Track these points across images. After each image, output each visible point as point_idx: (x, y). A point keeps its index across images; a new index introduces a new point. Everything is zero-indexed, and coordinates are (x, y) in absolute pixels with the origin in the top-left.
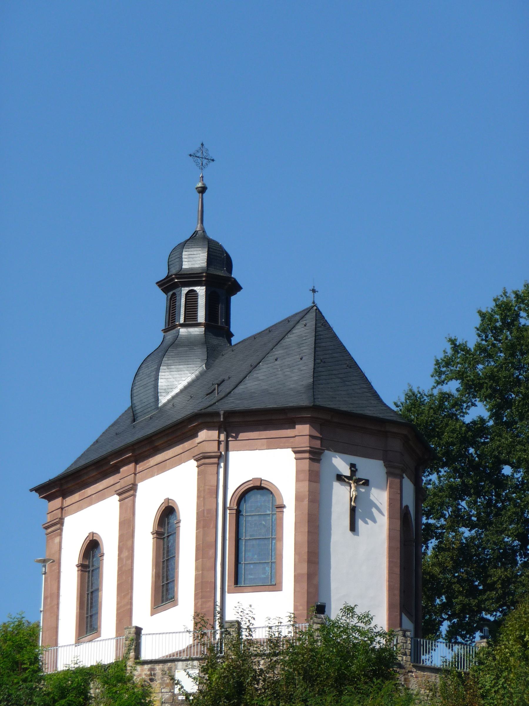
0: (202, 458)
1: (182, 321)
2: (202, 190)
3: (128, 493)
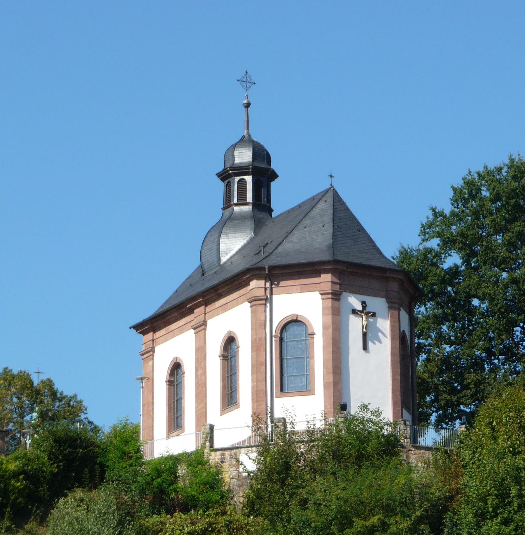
0: (253, 301)
1: (236, 201)
2: (248, 105)
3: (201, 327)
